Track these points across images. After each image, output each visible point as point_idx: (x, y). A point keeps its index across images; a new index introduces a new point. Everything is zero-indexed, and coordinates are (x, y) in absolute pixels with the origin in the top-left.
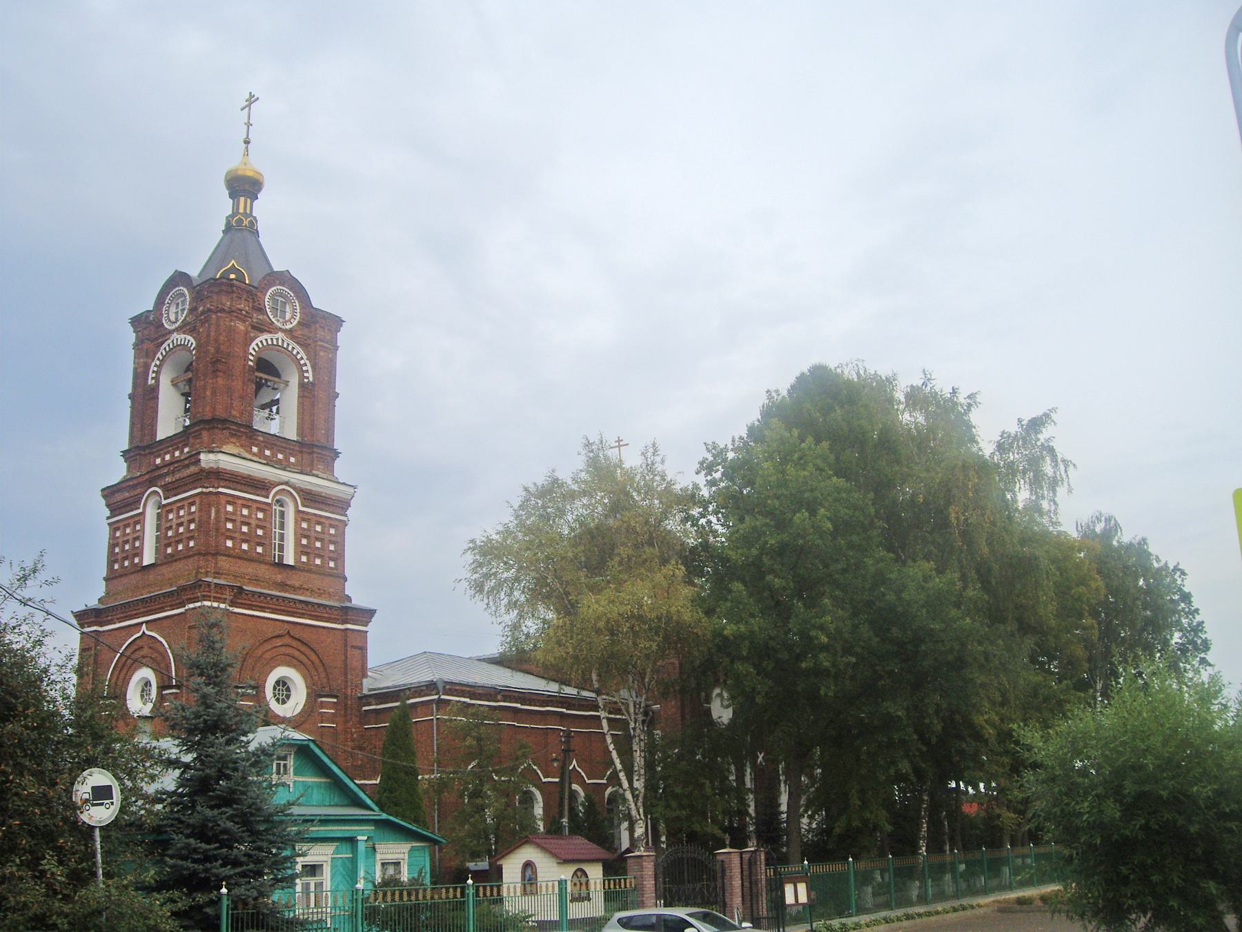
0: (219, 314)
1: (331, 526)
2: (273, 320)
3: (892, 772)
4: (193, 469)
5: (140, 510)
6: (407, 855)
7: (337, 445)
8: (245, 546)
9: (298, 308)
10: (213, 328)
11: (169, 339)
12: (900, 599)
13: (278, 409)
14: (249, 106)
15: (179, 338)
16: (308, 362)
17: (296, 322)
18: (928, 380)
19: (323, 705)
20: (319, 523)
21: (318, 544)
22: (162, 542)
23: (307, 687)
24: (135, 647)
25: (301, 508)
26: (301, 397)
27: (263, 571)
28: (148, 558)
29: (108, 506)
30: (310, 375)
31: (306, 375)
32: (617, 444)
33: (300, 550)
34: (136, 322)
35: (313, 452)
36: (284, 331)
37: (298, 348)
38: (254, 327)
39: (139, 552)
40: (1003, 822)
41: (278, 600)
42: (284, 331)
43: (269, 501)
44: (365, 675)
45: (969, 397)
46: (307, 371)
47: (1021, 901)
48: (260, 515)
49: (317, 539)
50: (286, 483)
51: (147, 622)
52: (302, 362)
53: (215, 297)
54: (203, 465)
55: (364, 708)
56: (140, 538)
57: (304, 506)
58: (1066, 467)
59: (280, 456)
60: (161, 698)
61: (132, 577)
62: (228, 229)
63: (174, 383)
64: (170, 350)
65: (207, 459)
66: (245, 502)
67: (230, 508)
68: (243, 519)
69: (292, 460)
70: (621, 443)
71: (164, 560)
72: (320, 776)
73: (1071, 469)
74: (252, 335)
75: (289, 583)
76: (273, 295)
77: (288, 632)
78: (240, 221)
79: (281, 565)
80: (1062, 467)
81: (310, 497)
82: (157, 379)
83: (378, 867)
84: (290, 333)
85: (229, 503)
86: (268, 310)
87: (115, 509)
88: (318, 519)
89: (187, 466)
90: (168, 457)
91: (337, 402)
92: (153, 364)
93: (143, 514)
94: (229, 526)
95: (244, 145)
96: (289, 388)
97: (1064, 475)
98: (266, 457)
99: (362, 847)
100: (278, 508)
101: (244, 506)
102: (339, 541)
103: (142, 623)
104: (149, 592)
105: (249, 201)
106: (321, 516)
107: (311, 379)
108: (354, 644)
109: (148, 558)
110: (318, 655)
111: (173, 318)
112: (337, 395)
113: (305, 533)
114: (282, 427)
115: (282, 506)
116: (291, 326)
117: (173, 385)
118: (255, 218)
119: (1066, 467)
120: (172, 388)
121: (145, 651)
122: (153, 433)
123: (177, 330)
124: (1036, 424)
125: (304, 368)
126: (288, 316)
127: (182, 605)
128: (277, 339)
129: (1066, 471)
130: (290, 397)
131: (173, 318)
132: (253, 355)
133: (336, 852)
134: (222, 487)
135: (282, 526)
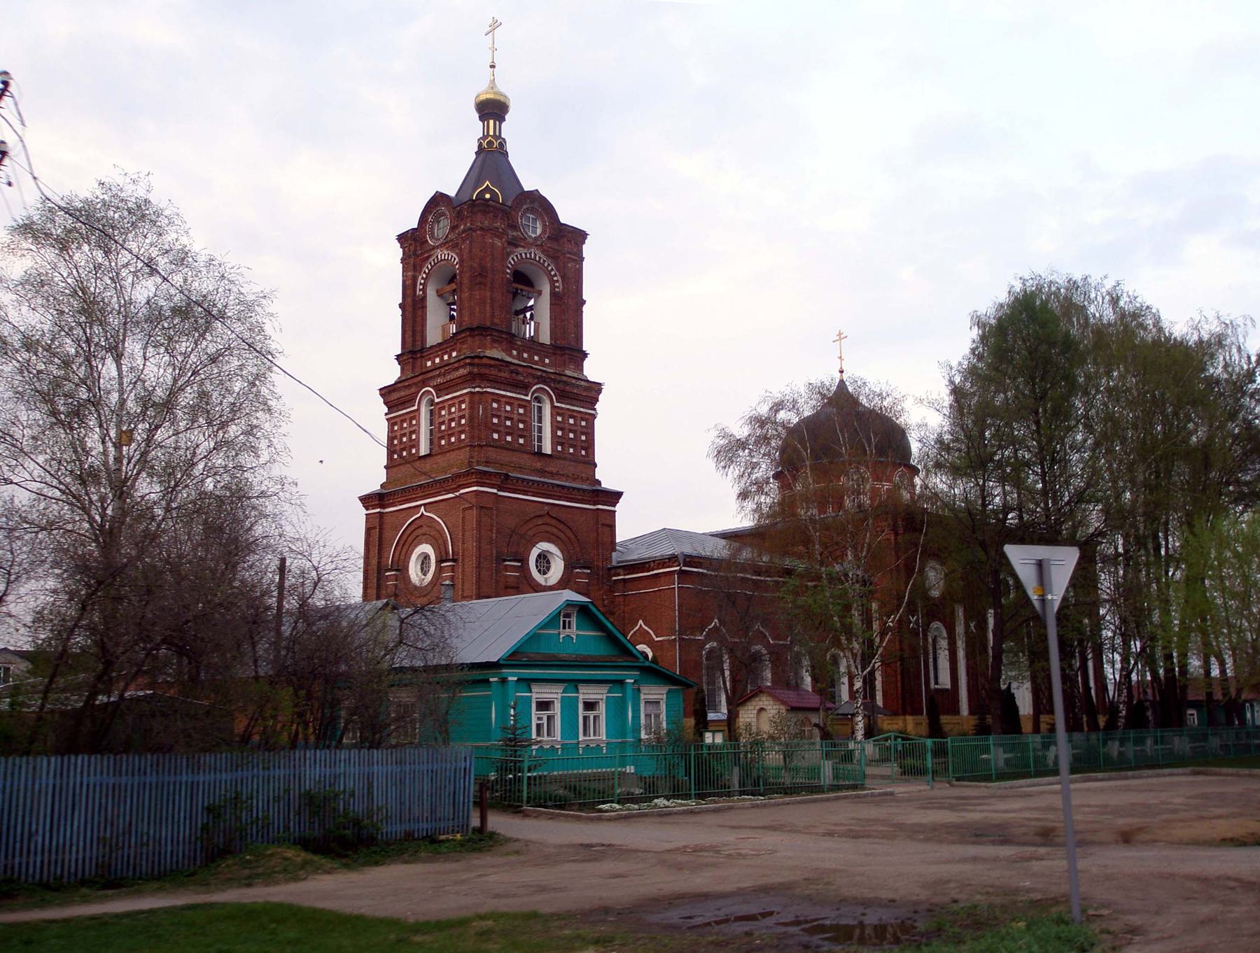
1: (583, 419)
5: (416, 408)
13: (532, 315)
20: (571, 417)
21: (571, 435)
25: (556, 404)
27: (525, 460)
29: (385, 403)
31: (557, 284)
33: (556, 441)
34: (402, 238)
38: (509, 243)
39: (416, 444)
44: (614, 549)
49: (571, 431)
62: (480, 151)
79: (540, 454)
82: (424, 290)
87: (391, 406)
88: (570, 413)
91: (585, 308)
92: (420, 277)
93: (418, 410)
94: (495, 421)
100: (536, 404)
103: (421, 505)
112: (584, 302)
117: (438, 296)
122: (424, 340)
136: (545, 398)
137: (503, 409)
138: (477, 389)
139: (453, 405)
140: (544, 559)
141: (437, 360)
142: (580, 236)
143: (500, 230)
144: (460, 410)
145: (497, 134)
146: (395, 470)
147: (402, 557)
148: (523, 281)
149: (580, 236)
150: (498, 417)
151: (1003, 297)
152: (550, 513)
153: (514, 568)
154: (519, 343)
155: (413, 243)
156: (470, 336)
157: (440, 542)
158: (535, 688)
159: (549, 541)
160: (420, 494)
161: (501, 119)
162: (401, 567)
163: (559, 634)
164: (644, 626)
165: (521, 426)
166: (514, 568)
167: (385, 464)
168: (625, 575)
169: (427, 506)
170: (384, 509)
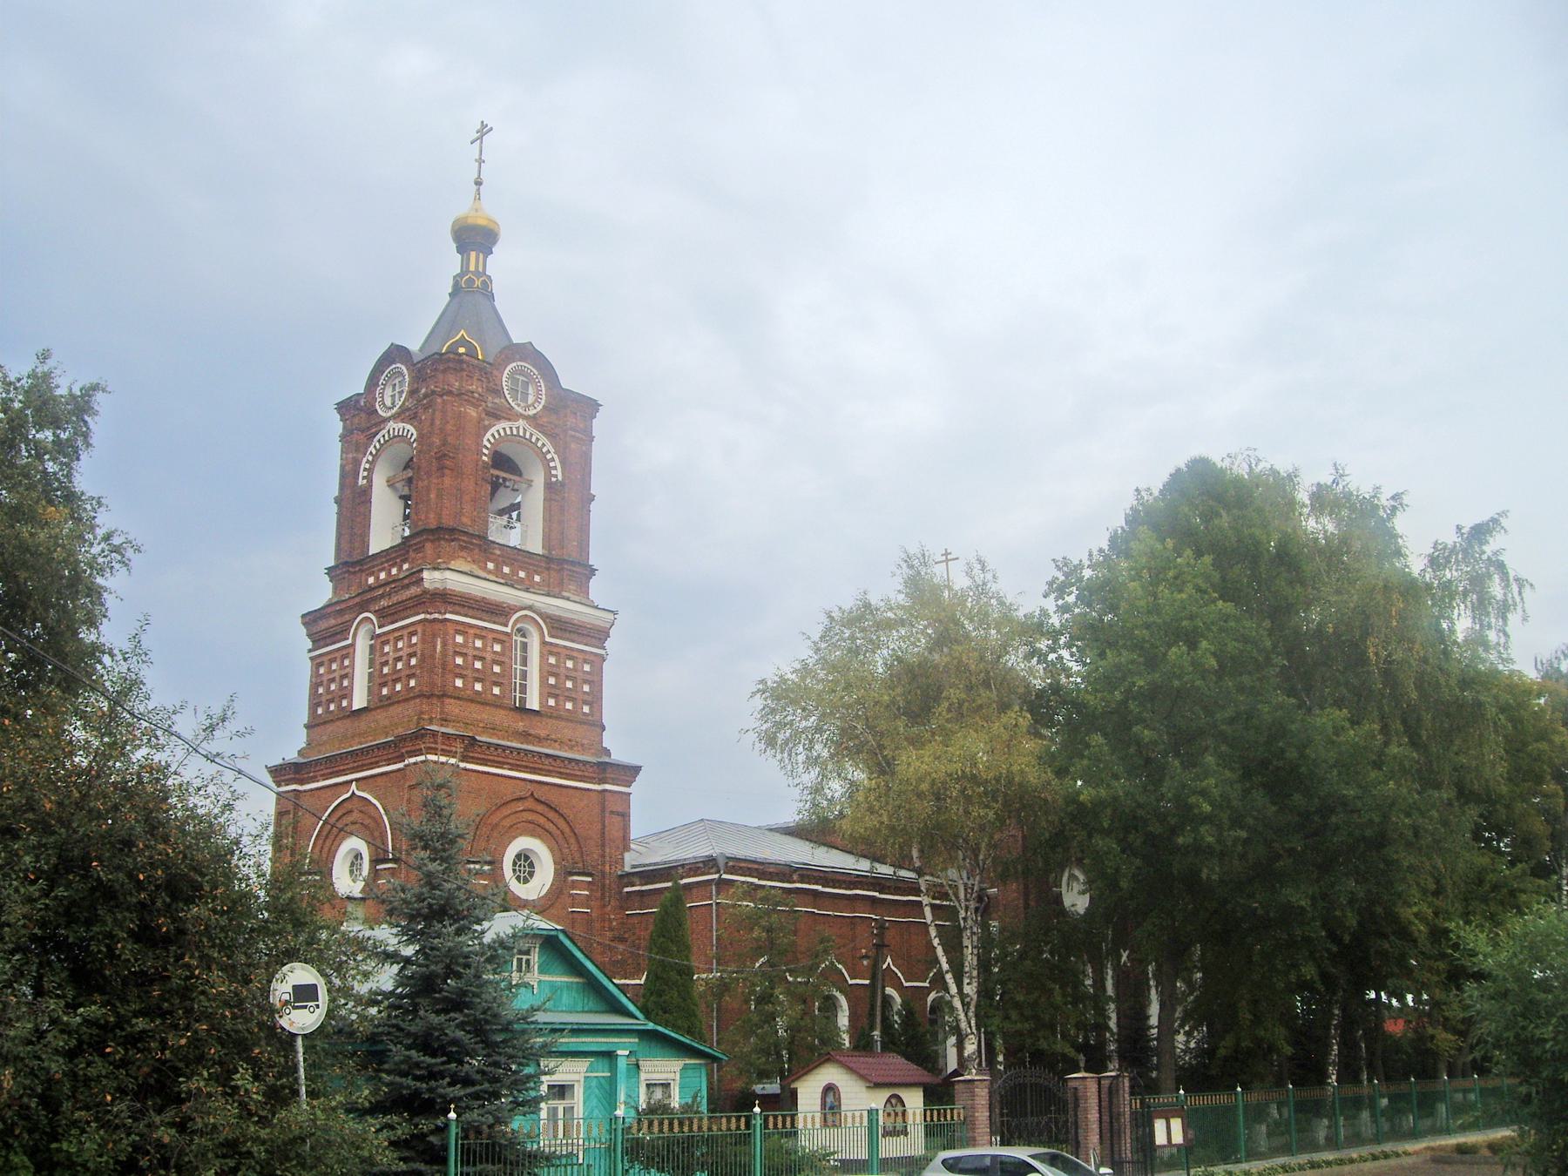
0: (445, 397)
1: (585, 661)
3: (1293, 978)
6: (678, 1075)
10: (438, 414)
11: (384, 428)
12: (1303, 756)
13: (519, 515)
14: (481, 138)
15: (395, 427)
16: (556, 457)
18: (1340, 474)
19: (574, 885)
21: (569, 684)
22: (377, 681)
25: (548, 639)
26: (548, 500)
27: (501, 717)
28: (359, 701)
29: (309, 635)
30: (559, 472)
31: (553, 472)
32: (944, 558)
33: (547, 691)
35: (562, 569)
36: (526, 418)
37: (543, 439)
38: (488, 414)
39: (347, 693)
40: (1438, 1047)
42: (526, 418)
43: (508, 630)
45: (1393, 498)
46: (555, 468)
47: (1462, 1150)
48: (497, 648)
49: (568, 678)
50: (530, 608)
51: (357, 780)
53: (440, 376)
54: (427, 585)
55: (626, 890)
58: (1521, 587)
60: (375, 874)
63: (391, 484)
65: (432, 579)
66: (478, 632)
67: (459, 639)
68: (476, 653)
69: (537, 578)
70: (949, 557)
71: (378, 704)
73: (1527, 591)
74: (487, 423)
77: (532, 794)
78: (470, 281)
79: (523, 710)
80: (1515, 588)
81: (559, 626)
82: (369, 479)
83: (643, 1090)
84: (533, 420)
86: (506, 392)
88: (568, 652)
89: (407, 587)
90: (383, 575)
91: (593, 506)
93: (353, 645)
94: (459, 661)
95: (475, 187)
97: (1518, 599)
98: (504, 576)
99: (622, 1064)
101: (477, 636)
102: (596, 680)
103: (351, 781)
105: (481, 256)
106: (572, 649)
107: (560, 478)
109: (359, 701)
111: (388, 402)
112: (593, 498)
114: (524, 536)
115: (524, 636)
116: (535, 411)
119: (1521, 587)
123: (395, 417)
124: (1480, 532)
125: (552, 464)
126: (531, 399)
127: (401, 758)
128: (518, 428)
129: (1520, 593)
130: (534, 500)
131: (388, 402)
132: (487, 448)
135: (524, 662)
137: (471, 645)
145: (481, 270)
154: (498, 552)
161: (488, 252)
165: (497, 669)
168: (642, 885)
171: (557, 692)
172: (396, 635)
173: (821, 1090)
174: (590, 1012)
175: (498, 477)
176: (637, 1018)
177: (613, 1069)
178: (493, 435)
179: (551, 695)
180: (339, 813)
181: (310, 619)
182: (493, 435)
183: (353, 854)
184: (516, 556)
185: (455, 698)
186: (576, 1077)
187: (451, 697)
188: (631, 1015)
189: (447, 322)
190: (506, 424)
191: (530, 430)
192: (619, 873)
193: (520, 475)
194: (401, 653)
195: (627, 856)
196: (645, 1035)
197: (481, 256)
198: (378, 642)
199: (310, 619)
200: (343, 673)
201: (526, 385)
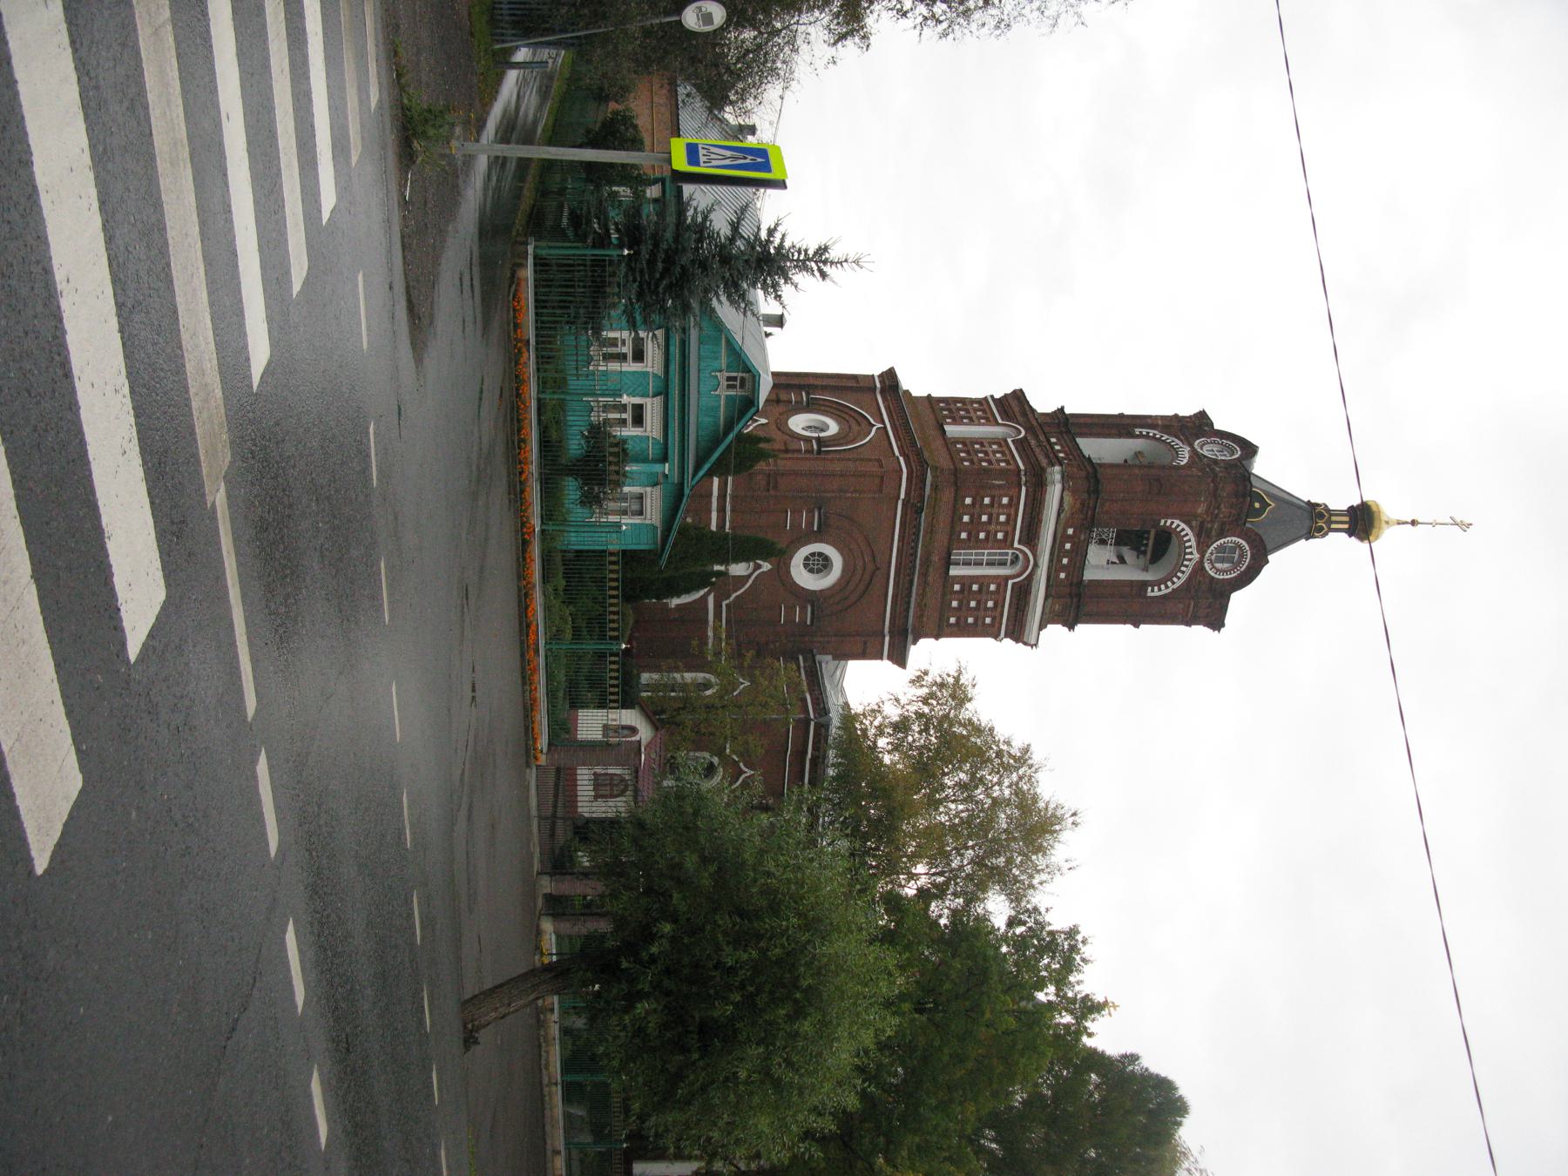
1: (994, 619)
2: (1212, 548)
4: (1044, 462)
5: (1000, 421)
6: (649, 522)
7: (1080, 628)
8: (966, 518)
9: (1229, 577)
16: (1170, 590)
17: (1213, 574)
19: (803, 610)
21: (973, 604)
22: (967, 443)
23: (821, 591)
24: (860, 419)
25: (1010, 582)
26: (1130, 583)
27: (941, 538)
29: (1006, 395)
30: (1156, 593)
33: (966, 582)
34: (1202, 415)
36: (1201, 561)
37: (1184, 578)
38: (1202, 524)
41: (911, 555)
42: (1201, 561)
43: (1016, 545)
44: (834, 659)
48: (1000, 536)
49: (978, 603)
50: (1036, 565)
51: (885, 428)
52: (1169, 583)
54: (1049, 470)
55: (801, 658)
56: (971, 421)
57: (1014, 584)
59: (1065, 561)
60: (808, 440)
61: (932, 416)
62: (1312, 506)
63: (1138, 454)
64: (1172, 446)
65: (1055, 473)
66: (1012, 517)
67: (1005, 500)
68: (995, 516)
69: (1062, 575)
71: (949, 443)
72: (725, 421)
74: (1194, 523)
75: (931, 570)
76: (1240, 546)
77: (878, 569)
79: (948, 563)
81: (1023, 593)
82: (1141, 436)
83: (637, 490)
85: (1011, 500)
86: (1222, 541)
89: (1047, 456)
91: (1129, 627)
92: (1156, 432)
93: (997, 424)
94: (987, 501)
95: (1409, 520)
96: (1140, 572)
99: (657, 468)
100: (1009, 558)
101: (1008, 517)
103: (883, 422)
104: (916, 430)
105: (1346, 526)
106: (1003, 606)
108: (868, 644)
110: (858, 600)
113: (985, 588)
115: (1013, 563)
116: (1208, 569)
117: (1136, 454)
118: (1326, 534)
120: (1132, 453)
121: (855, 427)
122: (1083, 435)
125: (1163, 587)
126: (1219, 566)
127: (902, 453)
128: (1191, 553)
130: (1129, 573)
131: (1206, 447)
133: (655, 375)
134: (1027, 491)
135: (990, 564)
136: (1018, 568)
137: (1001, 511)
138: (1024, 479)
139: (1003, 453)
140: (819, 564)
141: (1057, 447)
142: (1216, 622)
143: (1216, 511)
144: (999, 461)
145: (1333, 526)
146: (927, 404)
147: (823, 408)
148: (1158, 546)
149: (1216, 622)
150: (992, 505)
151: (1163, 1075)
152: (878, 572)
153: (810, 523)
154: (1082, 537)
155: (1199, 425)
156: (1088, 473)
157: (842, 441)
158: (658, 401)
159: (844, 570)
160: (897, 423)
161: (1351, 532)
162: (811, 407)
163: (721, 371)
164: (742, 687)
165: (982, 536)
166: (810, 523)
167: (933, 395)
168: (805, 667)
169: (883, 431)
170: (881, 393)
171: (964, 608)
172: (1007, 452)
173: (633, 724)
174: (697, 440)
175: (1148, 539)
176: (692, 479)
177: (655, 461)
178: (1183, 530)
179: (963, 586)
180: (856, 416)
181: (1019, 396)
182: (1183, 530)
183: (824, 427)
184: (1079, 557)
185: (955, 497)
186: (649, 429)
187: (956, 493)
188: (697, 468)
189: (1286, 502)
190: (1193, 543)
191: (1191, 564)
192: (815, 651)
193: (1151, 563)
194: (991, 455)
195: (829, 657)
196: (681, 484)
197: (1346, 526)
198: (1002, 442)
199: (1019, 396)
200: (974, 418)
201: (1231, 560)
